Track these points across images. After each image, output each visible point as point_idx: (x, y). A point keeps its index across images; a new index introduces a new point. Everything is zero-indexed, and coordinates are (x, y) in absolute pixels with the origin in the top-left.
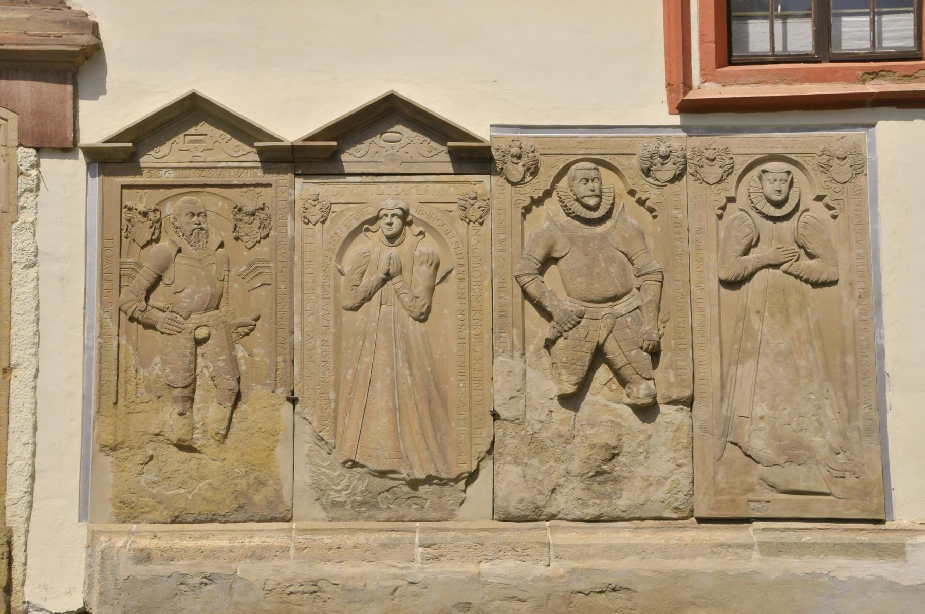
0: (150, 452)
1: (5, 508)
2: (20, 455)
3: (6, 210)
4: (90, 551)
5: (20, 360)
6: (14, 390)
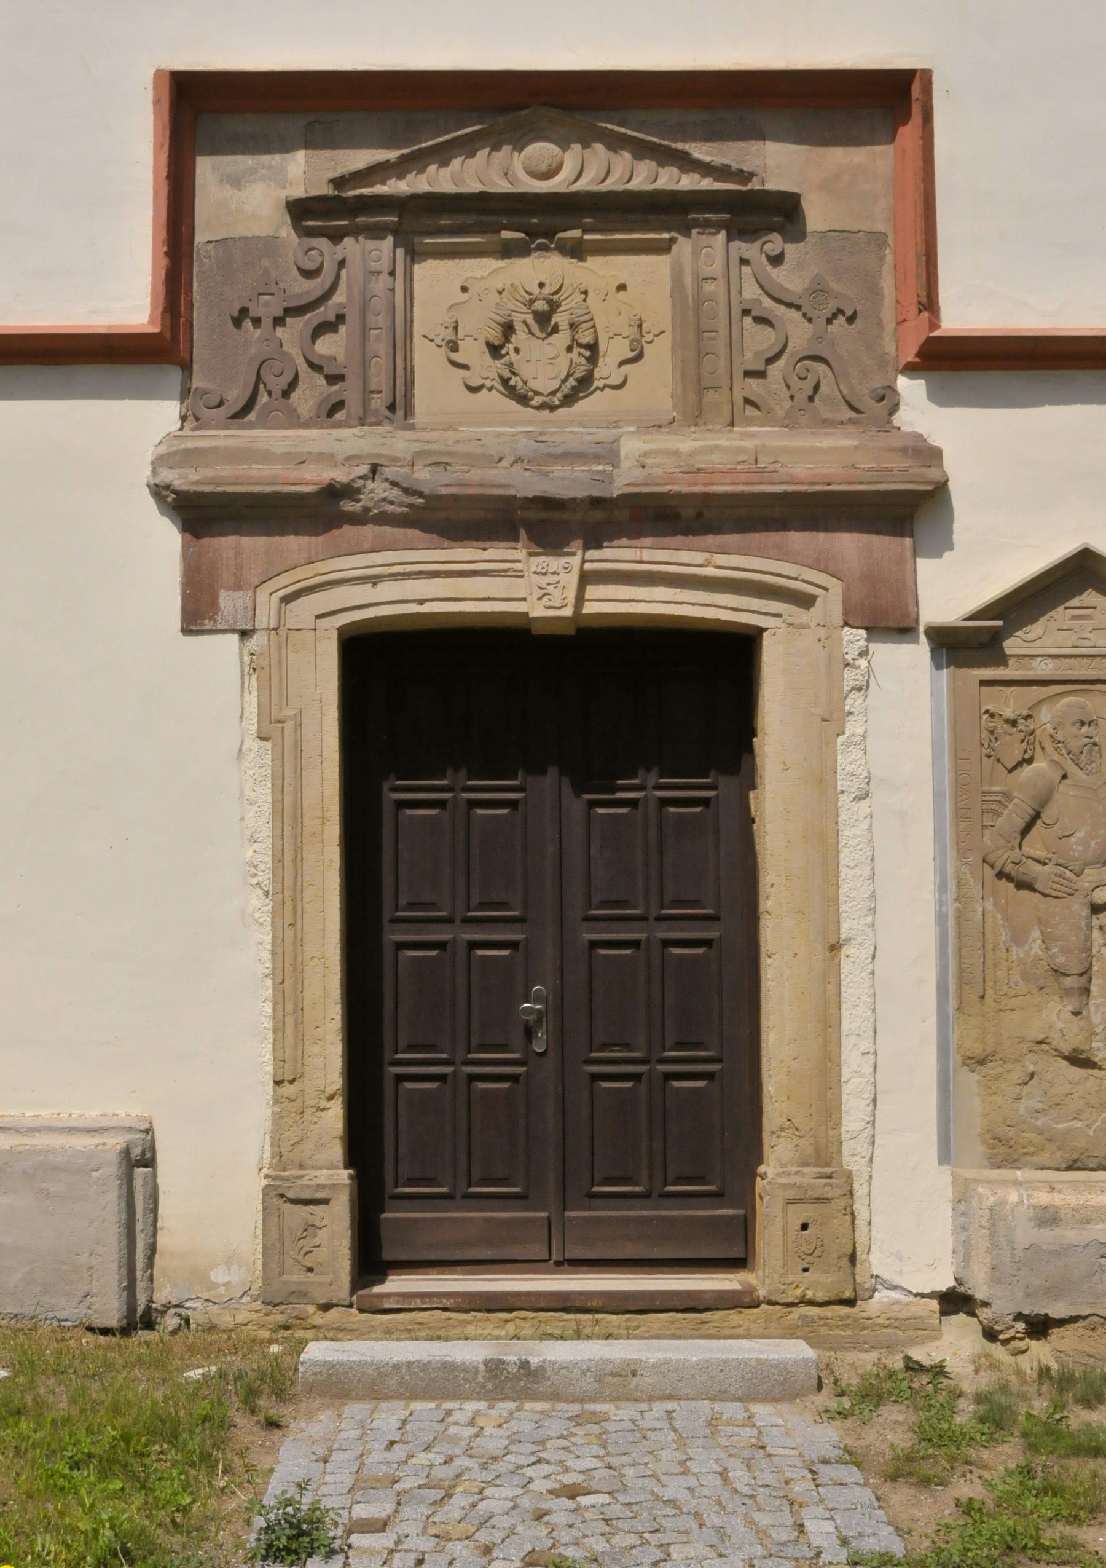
0: (1031, 1068)
1: (841, 1143)
2: (859, 1069)
3: (828, 718)
4: (962, 1207)
5: (853, 932)
6: (846, 976)
